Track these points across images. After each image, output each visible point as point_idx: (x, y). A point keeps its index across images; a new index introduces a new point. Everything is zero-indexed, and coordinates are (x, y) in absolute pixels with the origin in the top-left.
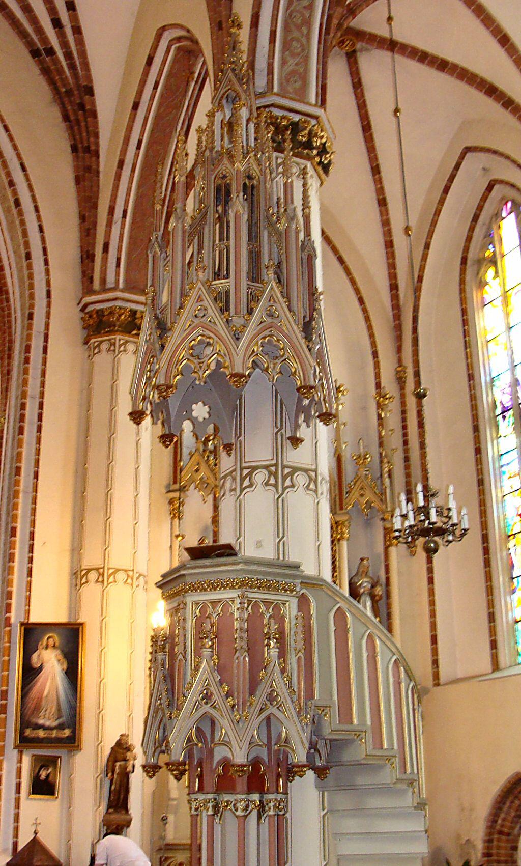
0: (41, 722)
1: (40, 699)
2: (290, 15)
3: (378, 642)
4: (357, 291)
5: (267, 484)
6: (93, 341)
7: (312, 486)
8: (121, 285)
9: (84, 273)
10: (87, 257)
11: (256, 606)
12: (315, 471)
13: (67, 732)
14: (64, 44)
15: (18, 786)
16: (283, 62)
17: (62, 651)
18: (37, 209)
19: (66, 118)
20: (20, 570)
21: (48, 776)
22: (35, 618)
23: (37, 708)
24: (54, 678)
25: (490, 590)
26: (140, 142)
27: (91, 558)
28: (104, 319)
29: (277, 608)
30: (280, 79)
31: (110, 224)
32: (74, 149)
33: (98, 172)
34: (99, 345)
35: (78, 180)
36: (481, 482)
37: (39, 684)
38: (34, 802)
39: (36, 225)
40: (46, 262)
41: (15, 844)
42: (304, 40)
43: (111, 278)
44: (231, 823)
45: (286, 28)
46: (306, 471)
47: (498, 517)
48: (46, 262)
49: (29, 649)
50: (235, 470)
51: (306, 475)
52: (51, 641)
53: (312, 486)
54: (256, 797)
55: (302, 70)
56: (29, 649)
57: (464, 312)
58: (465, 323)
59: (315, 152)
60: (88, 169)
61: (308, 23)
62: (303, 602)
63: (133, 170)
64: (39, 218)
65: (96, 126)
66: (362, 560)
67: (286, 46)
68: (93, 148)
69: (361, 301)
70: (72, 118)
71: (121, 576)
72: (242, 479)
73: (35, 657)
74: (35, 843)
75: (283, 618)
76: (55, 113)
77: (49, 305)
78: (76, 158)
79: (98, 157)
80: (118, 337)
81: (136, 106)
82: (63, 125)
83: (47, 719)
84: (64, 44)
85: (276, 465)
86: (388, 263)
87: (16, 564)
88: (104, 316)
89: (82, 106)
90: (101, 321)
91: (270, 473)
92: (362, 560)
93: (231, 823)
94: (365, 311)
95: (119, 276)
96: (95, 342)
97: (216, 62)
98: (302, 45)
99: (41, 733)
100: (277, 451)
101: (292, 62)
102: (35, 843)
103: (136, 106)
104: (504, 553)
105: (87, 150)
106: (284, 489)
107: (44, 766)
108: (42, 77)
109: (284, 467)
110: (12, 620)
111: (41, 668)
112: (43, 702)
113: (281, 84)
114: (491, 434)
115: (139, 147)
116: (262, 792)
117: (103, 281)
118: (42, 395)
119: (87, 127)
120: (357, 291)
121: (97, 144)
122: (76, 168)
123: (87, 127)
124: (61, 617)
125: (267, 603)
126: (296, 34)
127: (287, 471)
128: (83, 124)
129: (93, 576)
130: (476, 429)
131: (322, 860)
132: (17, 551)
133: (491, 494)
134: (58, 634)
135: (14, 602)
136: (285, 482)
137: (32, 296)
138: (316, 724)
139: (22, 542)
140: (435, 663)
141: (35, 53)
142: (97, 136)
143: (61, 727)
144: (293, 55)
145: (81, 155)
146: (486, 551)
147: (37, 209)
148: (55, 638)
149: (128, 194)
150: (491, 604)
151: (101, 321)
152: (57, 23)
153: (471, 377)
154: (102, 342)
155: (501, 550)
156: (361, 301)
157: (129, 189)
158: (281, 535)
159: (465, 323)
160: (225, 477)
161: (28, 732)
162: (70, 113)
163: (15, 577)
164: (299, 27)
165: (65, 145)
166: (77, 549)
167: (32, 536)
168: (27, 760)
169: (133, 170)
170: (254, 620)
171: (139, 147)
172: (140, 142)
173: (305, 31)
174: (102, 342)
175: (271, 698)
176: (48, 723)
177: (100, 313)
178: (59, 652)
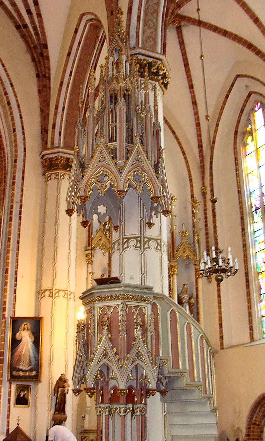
0: (21, 367)
1: (20, 356)
2: (148, 8)
3: (192, 327)
4: (182, 148)
5: (136, 247)
6: (47, 173)
7: (159, 248)
8: (62, 145)
9: (43, 139)
10: (44, 131)
11: (130, 308)
12: (160, 240)
13: (34, 373)
14: (33, 22)
15: (9, 400)
16: (144, 32)
17: (32, 332)
18: (19, 106)
19: (34, 60)
20: (10, 290)
21: (24, 395)
22: (18, 315)
23: (19, 361)
24: (27, 345)
25: (249, 301)
26: (71, 72)
27: (46, 284)
28: (53, 162)
29: (141, 309)
30: (142, 40)
31: (56, 114)
32: (38, 76)
33: (50, 88)
34: (50, 176)
35: (40, 92)
36: (245, 246)
37: (20, 348)
38: (17, 409)
39: (18, 114)
40: (24, 134)
41: (8, 430)
42: (155, 21)
43: (56, 142)
44: (118, 419)
45: (146, 14)
46: (156, 240)
47: (253, 263)
48: (24, 134)
49: (15, 330)
50: (119, 239)
51: (156, 242)
52: (26, 327)
53: (159, 248)
54: (130, 406)
55: (153, 36)
56: (15, 330)
57: (236, 159)
58: (236, 164)
59: (160, 77)
60: (45, 86)
61: (157, 12)
62: (154, 306)
63: (68, 87)
64: (20, 111)
65: (49, 64)
66: (184, 285)
67: (145, 24)
68: (47, 75)
69: (184, 153)
70: (37, 60)
71: (61, 293)
72: (123, 244)
73: (18, 335)
74: (18, 429)
75: (144, 315)
76: (28, 58)
77: (25, 155)
78: (39, 81)
79: (50, 80)
80: (60, 171)
81: (69, 54)
82: (32, 64)
83: (24, 366)
84: (33, 22)
85: (140, 237)
86: (197, 134)
87: (8, 287)
88: (53, 161)
89: (42, 54)
90: (51, 164)
91: (137, 241)
92: (184, 285)
93: (118, 419)
94: (186, 158)
95: (60, 140)
96: (48, 174)
97: (110, 32)
98: (154, 23)
99: (21, 374)
100: (141, 230)
101: (148, 31)
102: (18, 429)
103: (69, 54)
104: (257, 282)
105: (44, 76)
106: (144, 249)
107: (22, 390)
108: (21, 39)
109: (144, 238)
110: (6, 316)
111: (21, 340)
112: (22, 358)
113: (143, 43)
114: (250, 221)
115: (71, 75)
116: (133, 403)
117: (53, 143)
118: (21, 201)
119: (44, 65)
120: (182, 148)
121: (49, 74)
122: (39, 86)
123: (44, 65)
124: (31, 314)
125: (136, 307)
126: (150, 17)
127: (146, 240)
128: (42, 63)
129: (47, 293)
130: (242, 218)
131: (164, 438)
132: (9, 281)
133: (250, 252)
134: (30, 323)
135: (7, 306)
136: (145, 245)
137: (16, 151)
138: (161, 369)
139: (11, 276)
140: (221, 337)
141: (18, 27)
142: (49, 69)
143: (31, 370)
144: (149, 28)
145: (41, 79)
146: (247, 280)
147: (19, 106)
148: (28, 325)
149: (65, 99)
150: (250, 308)
151: (51, 164)
152: (29, 12)
153: (239, 192)
154: (52, 174)
155: (255, 280)
156: (184, 153)
157: (66, 96)
158: (143, 273)
159: (236, 164)
160: (114, 243)
161: (14, 373)
162: (36, 57)
163: (8, 294)
164: (152, 14)
165: (33, 74)
166: (39, 280)
167: (16, 273)
168: (14, 387)
169: (68, 87)
170: (129, 316)
171: (71, 75)
172: (71, 72)
173: (155, 16)
174: (52, 174)
175: (138, 355)
176: (24, 368)
177: (51, 159)
178: (30, 332)
